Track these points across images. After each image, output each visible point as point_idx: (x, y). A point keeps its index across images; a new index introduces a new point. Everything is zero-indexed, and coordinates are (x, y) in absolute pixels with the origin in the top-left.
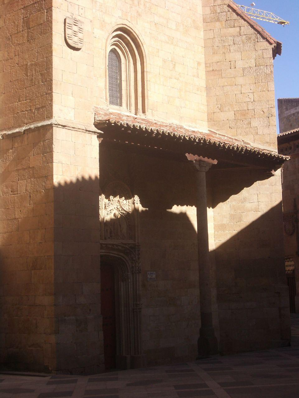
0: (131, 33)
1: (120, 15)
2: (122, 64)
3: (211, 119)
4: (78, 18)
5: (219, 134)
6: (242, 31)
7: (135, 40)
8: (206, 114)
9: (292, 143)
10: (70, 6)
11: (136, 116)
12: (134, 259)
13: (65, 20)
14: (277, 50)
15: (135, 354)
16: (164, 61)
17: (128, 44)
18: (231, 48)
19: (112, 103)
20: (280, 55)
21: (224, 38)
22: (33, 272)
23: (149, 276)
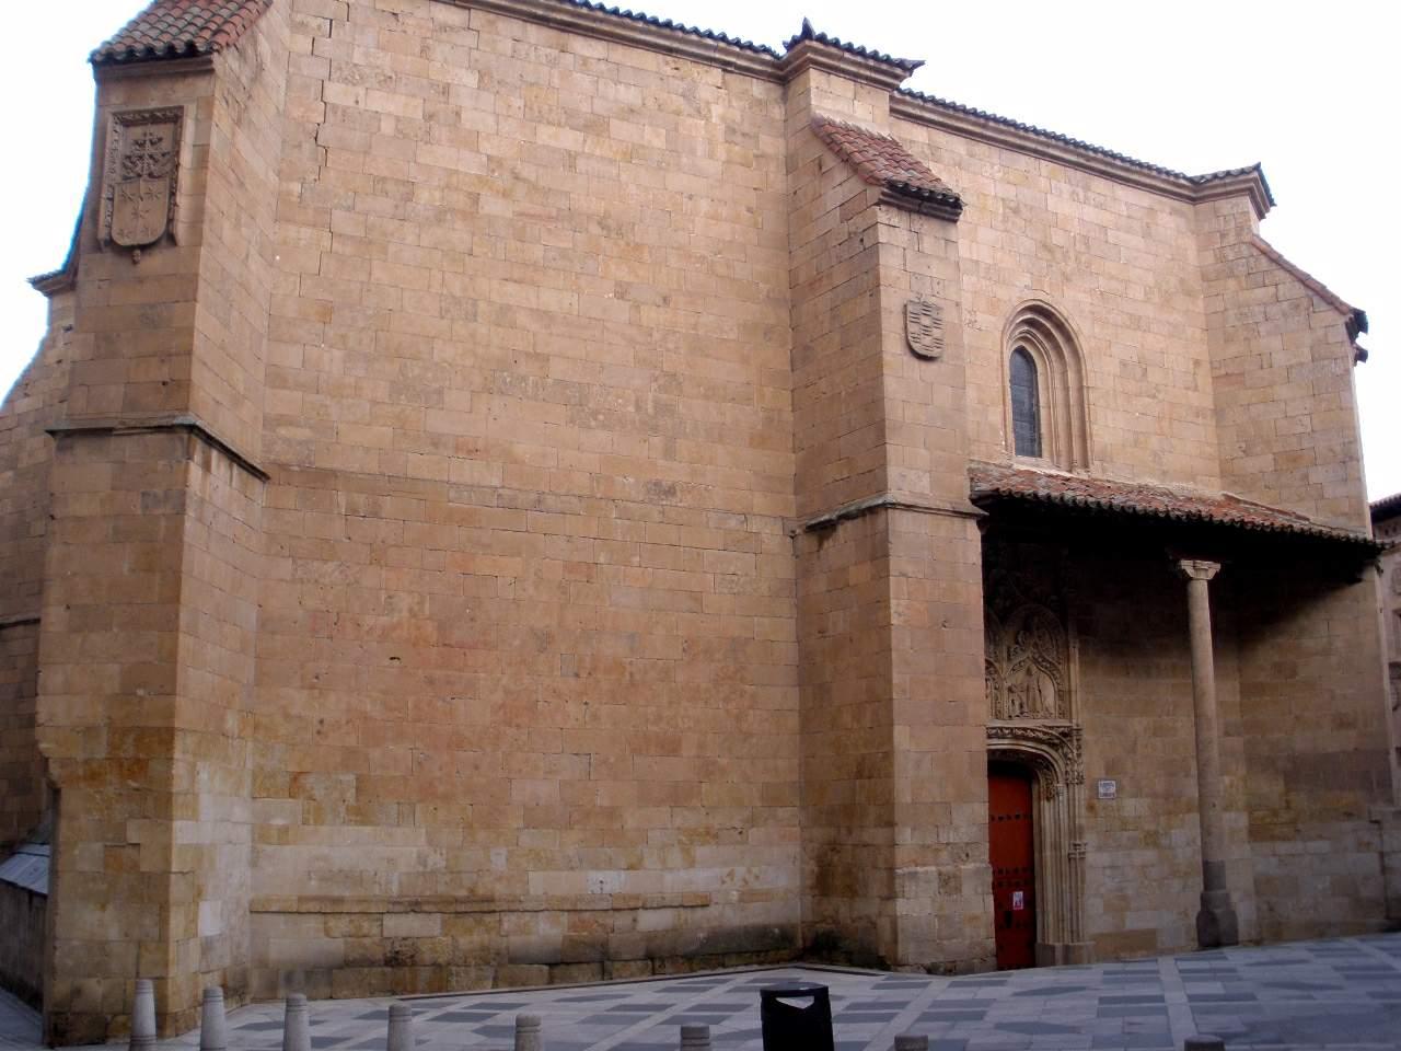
0: (1053, 314)
1: (1028, 282)
3: (1227, 473)
4: (932, 300)
5: (1246, 502)
6: (1281, 293)
7: (1060, 326)
8: (1218, 462)
11: (1068, 475)
12: (1070, 756)
13: (905, 306)
14: (164, 383)
16: (1124, 364)
17: (1048, 335)
18: (1260, 329)
19: (1021, 451)
21: (1246, 310)
22: (858, 782)
23: (1101, 790)
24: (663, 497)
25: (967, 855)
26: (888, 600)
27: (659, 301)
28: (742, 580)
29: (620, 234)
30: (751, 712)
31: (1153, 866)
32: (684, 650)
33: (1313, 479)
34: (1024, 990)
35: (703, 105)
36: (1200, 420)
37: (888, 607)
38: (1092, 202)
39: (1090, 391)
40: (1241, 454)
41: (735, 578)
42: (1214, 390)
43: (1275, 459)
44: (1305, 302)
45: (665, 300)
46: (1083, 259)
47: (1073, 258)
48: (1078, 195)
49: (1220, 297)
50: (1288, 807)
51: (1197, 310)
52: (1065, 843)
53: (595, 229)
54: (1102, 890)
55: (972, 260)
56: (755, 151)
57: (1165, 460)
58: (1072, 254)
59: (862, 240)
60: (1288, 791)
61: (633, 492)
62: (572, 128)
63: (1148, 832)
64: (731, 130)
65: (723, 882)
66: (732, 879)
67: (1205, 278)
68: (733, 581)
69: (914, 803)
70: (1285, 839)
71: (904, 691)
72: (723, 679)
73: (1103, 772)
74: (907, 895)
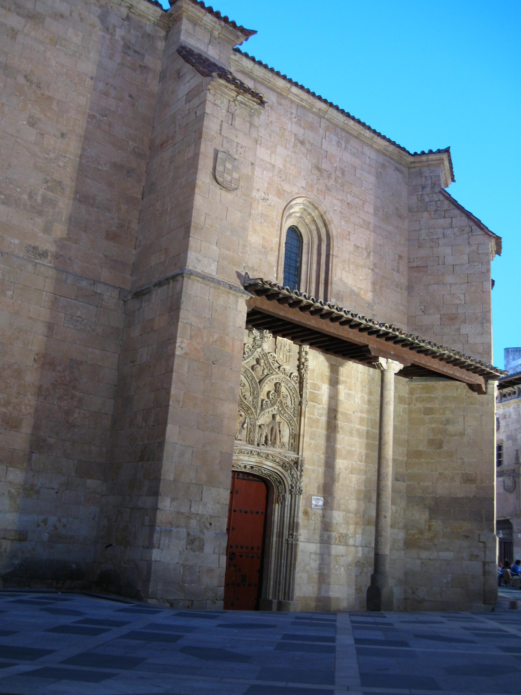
1: (304, 185)
2: (304, 244)
3: (411, 320)
6: (454, 223)
9: (516, 387)
10: (225, 141)
15: (284, 599)
18: (440, 242)
20: (500, 255)
22: (140, 464)
23: (314, 502)
24: (38, 257)
25: (211, 524)
26: (175, 338)
27: (58, 134)
28: (85, 321)
29: (38, 86)
30: (77, 410)
31: (342, 556)
32: (35, 360)
33: (463, 331)
34: (225, 623)
35: (111, 27)
36: (398, 290)
37: (175, 342)
38: (349, 151)
39: (334, 257)
40: (422, 313)
41: (80, 319)
42: (409, 275)
43: (441, 318)
44: (468, 229)
45: (63, 135)
46: (340, 181)
47: (334, 179)
48: (341, 144)
49: (418, 222)
50: (430, 529)
51: (404, 227)
52: (286, 532)
53: (21, 80)
54: (308, 568)
55: (271, 164)
56: (141, 63)
57: (375, 308)
58: (333, 176)
59: (196, 113)
60: (431, 518)
61: (16, 250)
62: (18, 14)
63: (342, 534)
64: (127, 47)
65: (39, 526)
66: (46, 525)
67: (410, 210)
68: (78, 321)
69: (175, 481)
70: (426, 549)
71: (178, 402)
72: (60, 384)
73: (316, 491)
74: (161, 546)
